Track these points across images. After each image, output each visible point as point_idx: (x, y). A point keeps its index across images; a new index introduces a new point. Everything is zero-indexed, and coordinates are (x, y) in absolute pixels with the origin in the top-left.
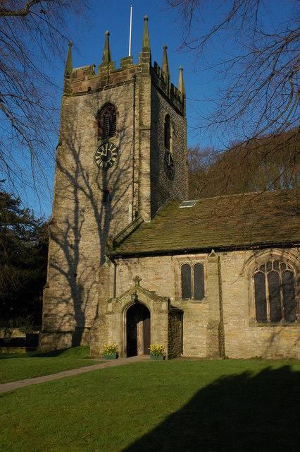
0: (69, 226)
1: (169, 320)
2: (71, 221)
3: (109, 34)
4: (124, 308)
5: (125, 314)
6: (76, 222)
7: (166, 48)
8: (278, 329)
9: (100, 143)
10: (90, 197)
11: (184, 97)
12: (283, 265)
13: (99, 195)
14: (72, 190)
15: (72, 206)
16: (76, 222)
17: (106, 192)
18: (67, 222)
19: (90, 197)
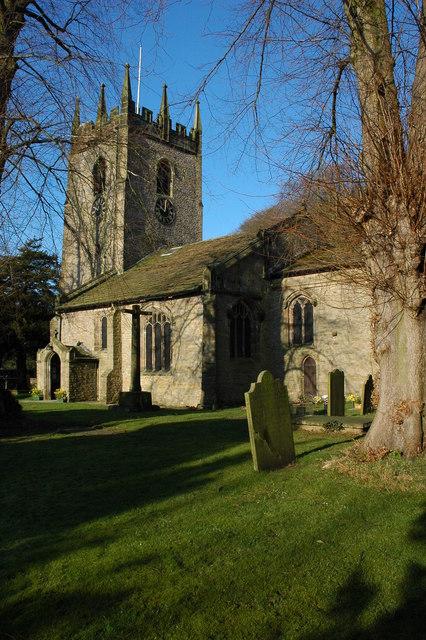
0: (74, 280)
1: (71, 369)
2: (75, 275)
3: (104, 86)
4: (47, 358)
5: (49, 362)
6: (79, 276)
7: (166, 87)
8: (156, 377)
9: (95, 198)
10: (88, 251)
11: (198, 133)
12: (164, 317)
13: (93, 249)
14: (75, 245)
15: (76, 261)
16: (79, 276)
17: (97, 245)
18: (72, 277)
19: (88, 251)
